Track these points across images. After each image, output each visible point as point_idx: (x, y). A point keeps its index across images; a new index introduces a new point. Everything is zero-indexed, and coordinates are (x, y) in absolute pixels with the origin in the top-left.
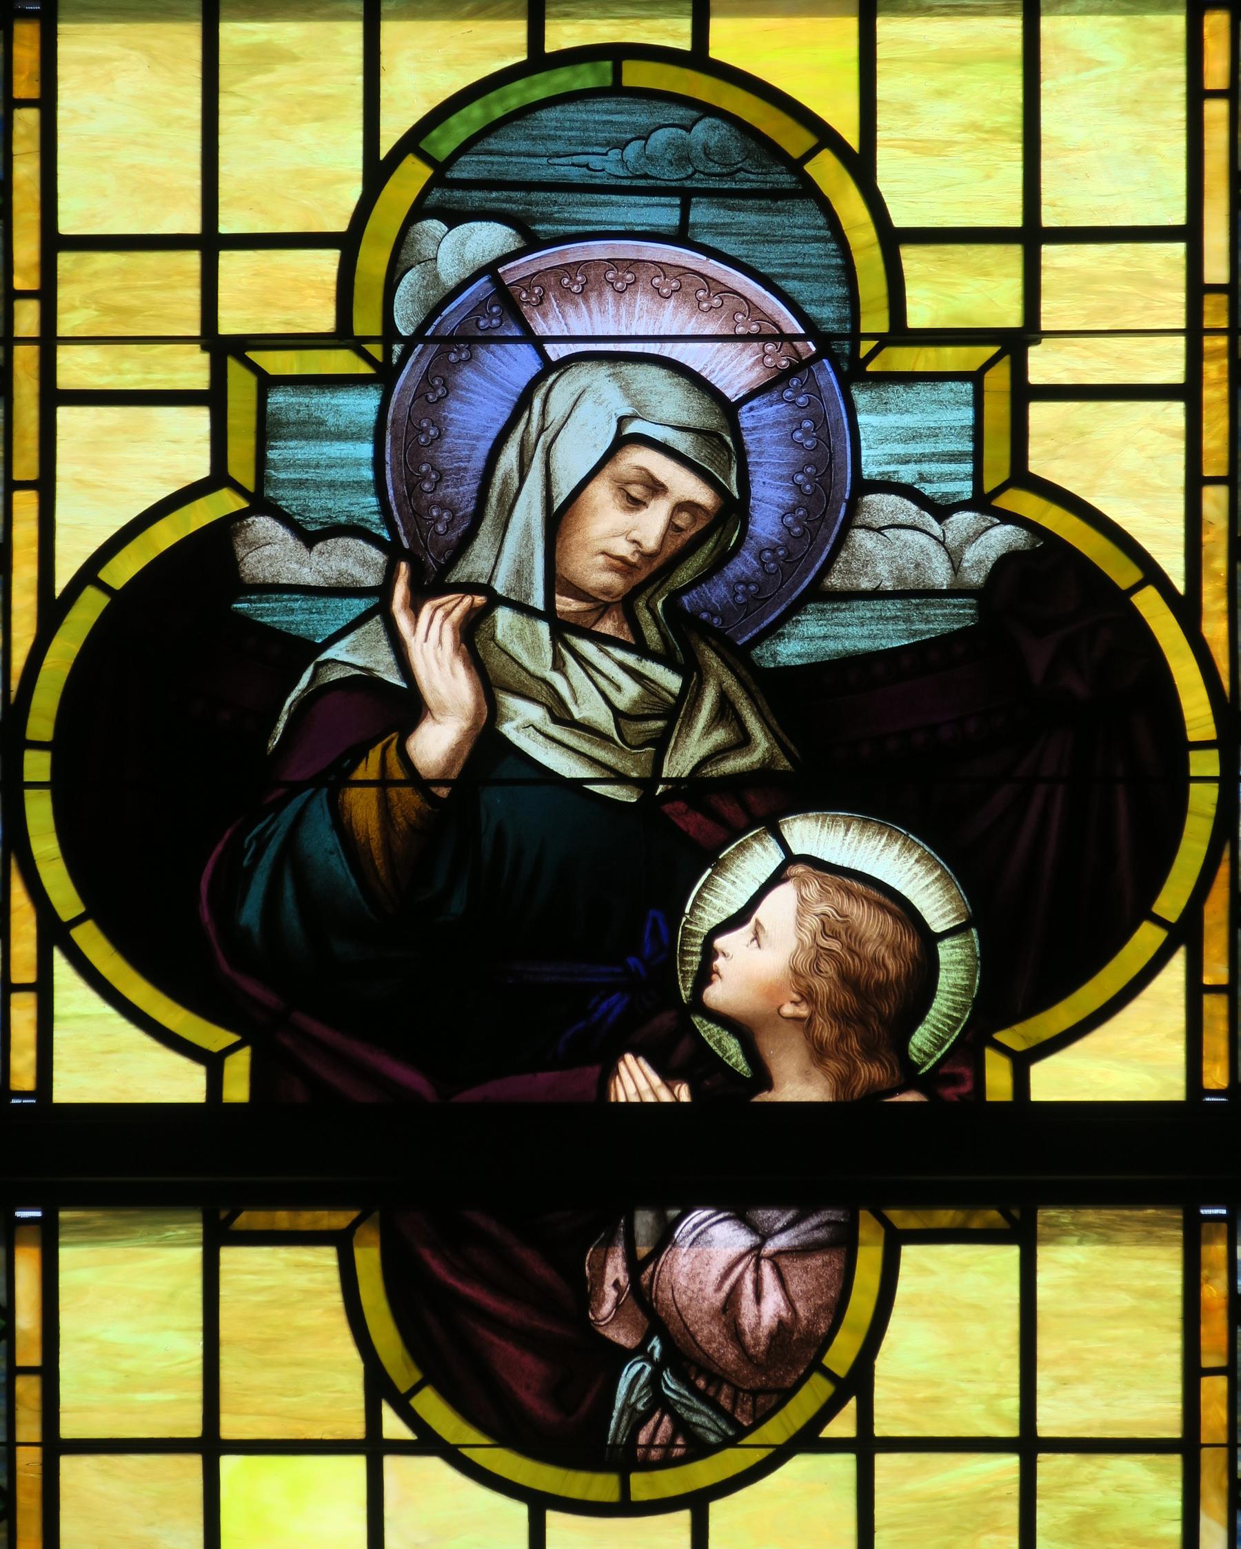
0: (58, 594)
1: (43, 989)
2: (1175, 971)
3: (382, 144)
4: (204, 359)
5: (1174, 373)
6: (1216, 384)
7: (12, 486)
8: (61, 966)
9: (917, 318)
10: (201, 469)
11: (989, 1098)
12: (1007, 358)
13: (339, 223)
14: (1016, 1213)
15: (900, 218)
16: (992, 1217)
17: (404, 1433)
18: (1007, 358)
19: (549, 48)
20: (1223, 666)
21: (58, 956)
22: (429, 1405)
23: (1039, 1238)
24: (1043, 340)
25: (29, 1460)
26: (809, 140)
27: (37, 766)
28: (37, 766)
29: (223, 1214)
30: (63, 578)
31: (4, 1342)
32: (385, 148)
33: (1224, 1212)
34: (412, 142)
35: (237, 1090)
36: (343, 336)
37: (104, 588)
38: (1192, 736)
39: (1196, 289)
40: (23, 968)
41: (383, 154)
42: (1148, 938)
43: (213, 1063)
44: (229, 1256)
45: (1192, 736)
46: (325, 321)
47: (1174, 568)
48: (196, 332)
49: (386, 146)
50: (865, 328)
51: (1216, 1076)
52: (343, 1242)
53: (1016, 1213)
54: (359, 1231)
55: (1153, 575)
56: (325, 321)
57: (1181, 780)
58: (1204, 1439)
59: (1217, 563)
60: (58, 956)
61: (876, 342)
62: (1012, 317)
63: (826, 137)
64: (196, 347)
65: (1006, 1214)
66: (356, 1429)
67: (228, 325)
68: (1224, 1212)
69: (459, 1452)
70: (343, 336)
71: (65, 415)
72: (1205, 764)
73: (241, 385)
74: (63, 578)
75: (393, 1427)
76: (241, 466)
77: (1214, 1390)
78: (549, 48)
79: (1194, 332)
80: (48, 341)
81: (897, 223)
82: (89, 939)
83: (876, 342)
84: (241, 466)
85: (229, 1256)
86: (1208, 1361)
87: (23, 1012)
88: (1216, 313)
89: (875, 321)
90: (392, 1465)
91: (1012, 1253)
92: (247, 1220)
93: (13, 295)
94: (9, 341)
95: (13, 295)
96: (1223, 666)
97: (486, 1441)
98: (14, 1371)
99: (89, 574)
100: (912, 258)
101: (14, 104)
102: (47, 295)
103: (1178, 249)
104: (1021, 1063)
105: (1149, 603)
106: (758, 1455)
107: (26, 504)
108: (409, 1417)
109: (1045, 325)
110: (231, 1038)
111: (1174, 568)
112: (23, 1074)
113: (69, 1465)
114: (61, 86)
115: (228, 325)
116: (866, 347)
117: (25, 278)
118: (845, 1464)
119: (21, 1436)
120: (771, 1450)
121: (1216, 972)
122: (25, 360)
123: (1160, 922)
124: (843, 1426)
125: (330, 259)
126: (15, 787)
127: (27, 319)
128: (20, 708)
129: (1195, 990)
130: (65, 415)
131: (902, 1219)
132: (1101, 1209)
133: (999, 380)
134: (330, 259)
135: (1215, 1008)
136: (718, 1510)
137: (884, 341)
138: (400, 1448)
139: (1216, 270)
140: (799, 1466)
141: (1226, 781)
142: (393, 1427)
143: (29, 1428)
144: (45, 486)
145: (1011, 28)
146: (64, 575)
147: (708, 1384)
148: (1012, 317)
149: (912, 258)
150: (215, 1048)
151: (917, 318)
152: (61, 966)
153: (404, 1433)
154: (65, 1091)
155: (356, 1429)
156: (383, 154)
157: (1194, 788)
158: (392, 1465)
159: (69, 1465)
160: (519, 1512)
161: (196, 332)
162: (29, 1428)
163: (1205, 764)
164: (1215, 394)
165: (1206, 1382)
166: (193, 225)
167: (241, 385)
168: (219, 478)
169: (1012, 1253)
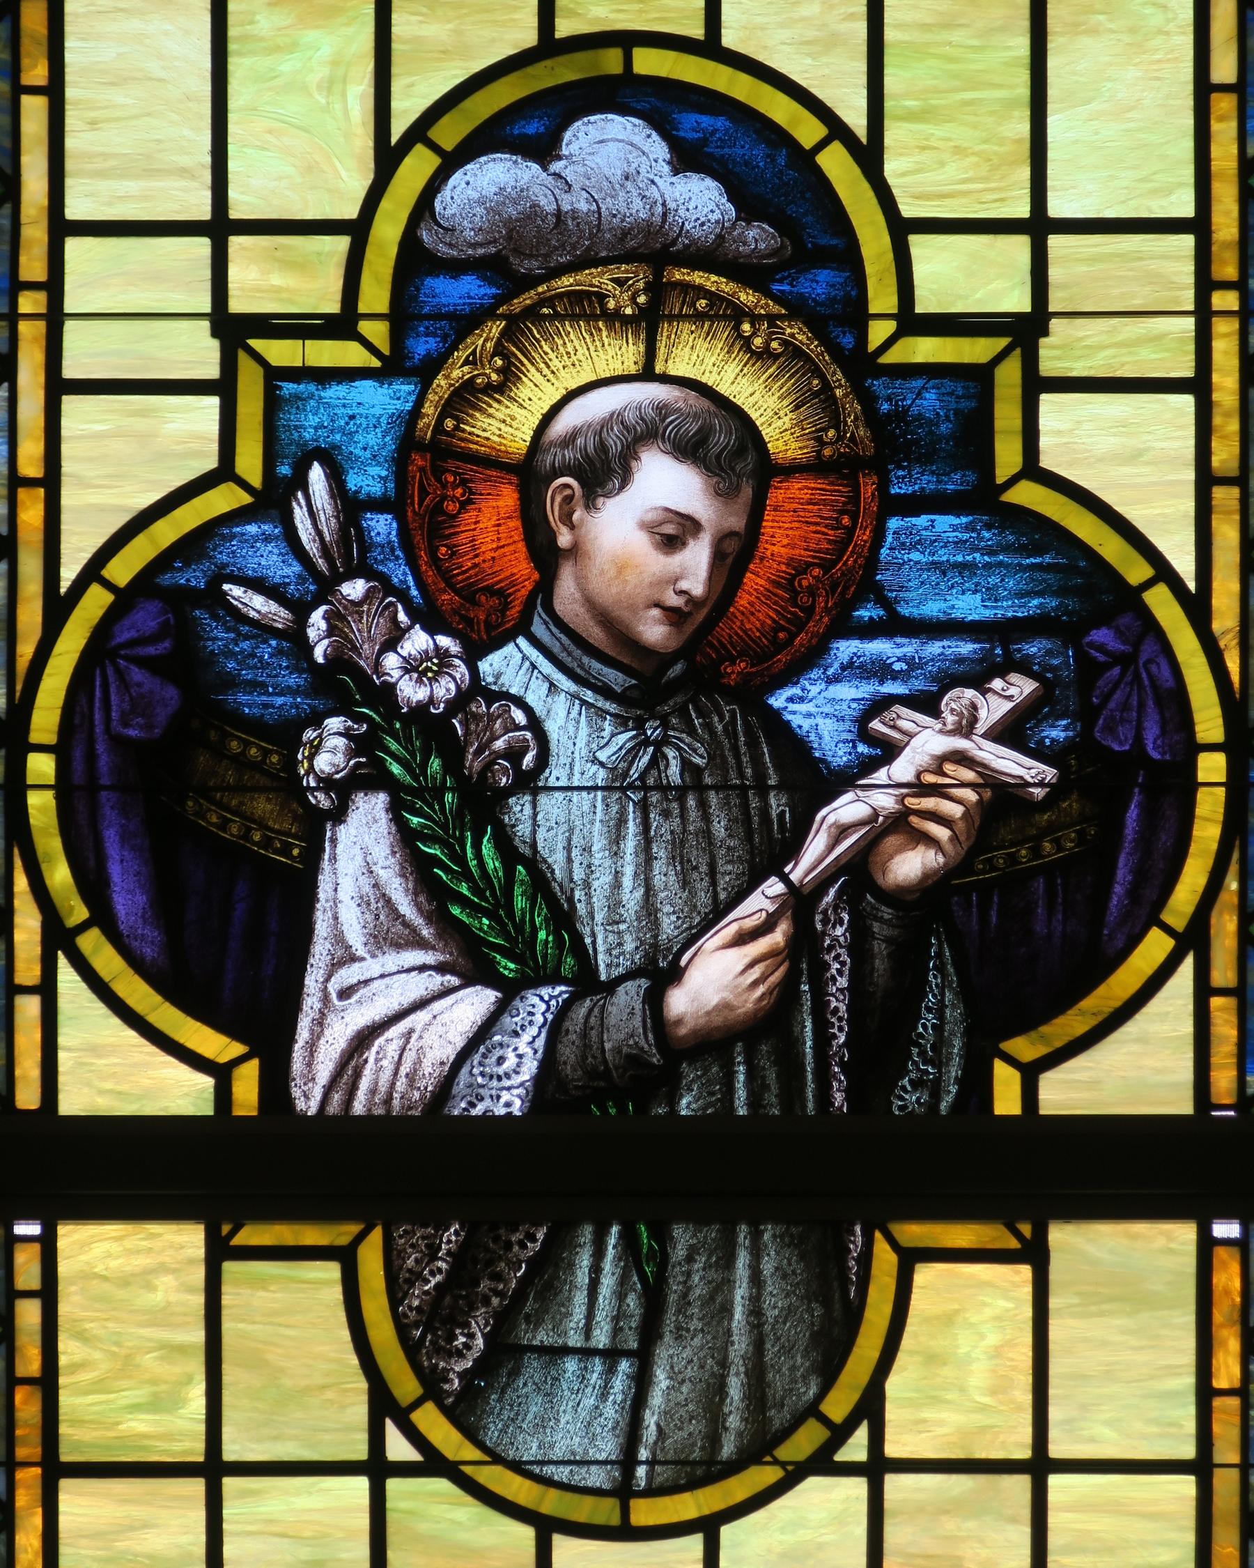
0: (63, 590)
1: (47, 990)
8: (67, 976)
11: (1042, 1112)
12: (1018, 352)
13: (351, 211)
14: (1026, 1229)
15: (908, 209)
18: (1018, 352)
21: (62, 961)
22: (430, 1420)
27: (41, 766)
28: (41, 766)
29: (226, 1229)
34: (419, 131)
36: (346, 1257)
37: (108, 585)
39: (1205, 284)
40: (28, 970)
42: (1155, 946)
43: (222, 1074)
44: (230, 1268)
47: (1184, 564)
51: (1224, 1081)
52: (346, 1257)
55: (1164, 572)
57: (1189, 786)
60: (62, 961)
62: (1018, 301)
63: (837, 129)
65: (1018, 1235)
67: (238, 304)
69: (460, 1470)
72: (1212, 767)
74: (68, 574)
75: (399, 1448)
79: (1204, 315)
80: (55, 318)
82: (93, 943)
85: (230, 1268)
86: (1220, 1382)
87: (29, 1008)
90: (394, 1486)
92: (250, 1235)
95: (15, 990)
98: (13, 1382)
99: (92, 572)
100: (920, 245)
101: (15, 990)
102: (54, 285)
103: (1187, 242)
104: (1030, 1074)
105: (1161, 603)
110: (238, 1049)
111: (1184, 564)
112: (28, 1097)
115: (238, 304)
117: (33, 266)
118: (858, 1487)
121: (1223, 972)
122: (31, 334)
124: (856, 1449)
125: (342, 243)
126: (17, 786)
128: (22, 707)
129: (1203, 990)
131: (914, 1233)
133: (1009, 376)
135: (1222, 1010)
138: (406, 1470)
141: (1235, 785)
142: (399, 1448)
143: (28, 1449)
149: (920, 245)
150: (223, 1059)
154: (71, 1103)
155: (359, 1450)
161: (206, 307)
162: (28, 1449)
163: (1212, 767)
165: (1217, 1402)
166: (203, 211)
168: (225, 472)
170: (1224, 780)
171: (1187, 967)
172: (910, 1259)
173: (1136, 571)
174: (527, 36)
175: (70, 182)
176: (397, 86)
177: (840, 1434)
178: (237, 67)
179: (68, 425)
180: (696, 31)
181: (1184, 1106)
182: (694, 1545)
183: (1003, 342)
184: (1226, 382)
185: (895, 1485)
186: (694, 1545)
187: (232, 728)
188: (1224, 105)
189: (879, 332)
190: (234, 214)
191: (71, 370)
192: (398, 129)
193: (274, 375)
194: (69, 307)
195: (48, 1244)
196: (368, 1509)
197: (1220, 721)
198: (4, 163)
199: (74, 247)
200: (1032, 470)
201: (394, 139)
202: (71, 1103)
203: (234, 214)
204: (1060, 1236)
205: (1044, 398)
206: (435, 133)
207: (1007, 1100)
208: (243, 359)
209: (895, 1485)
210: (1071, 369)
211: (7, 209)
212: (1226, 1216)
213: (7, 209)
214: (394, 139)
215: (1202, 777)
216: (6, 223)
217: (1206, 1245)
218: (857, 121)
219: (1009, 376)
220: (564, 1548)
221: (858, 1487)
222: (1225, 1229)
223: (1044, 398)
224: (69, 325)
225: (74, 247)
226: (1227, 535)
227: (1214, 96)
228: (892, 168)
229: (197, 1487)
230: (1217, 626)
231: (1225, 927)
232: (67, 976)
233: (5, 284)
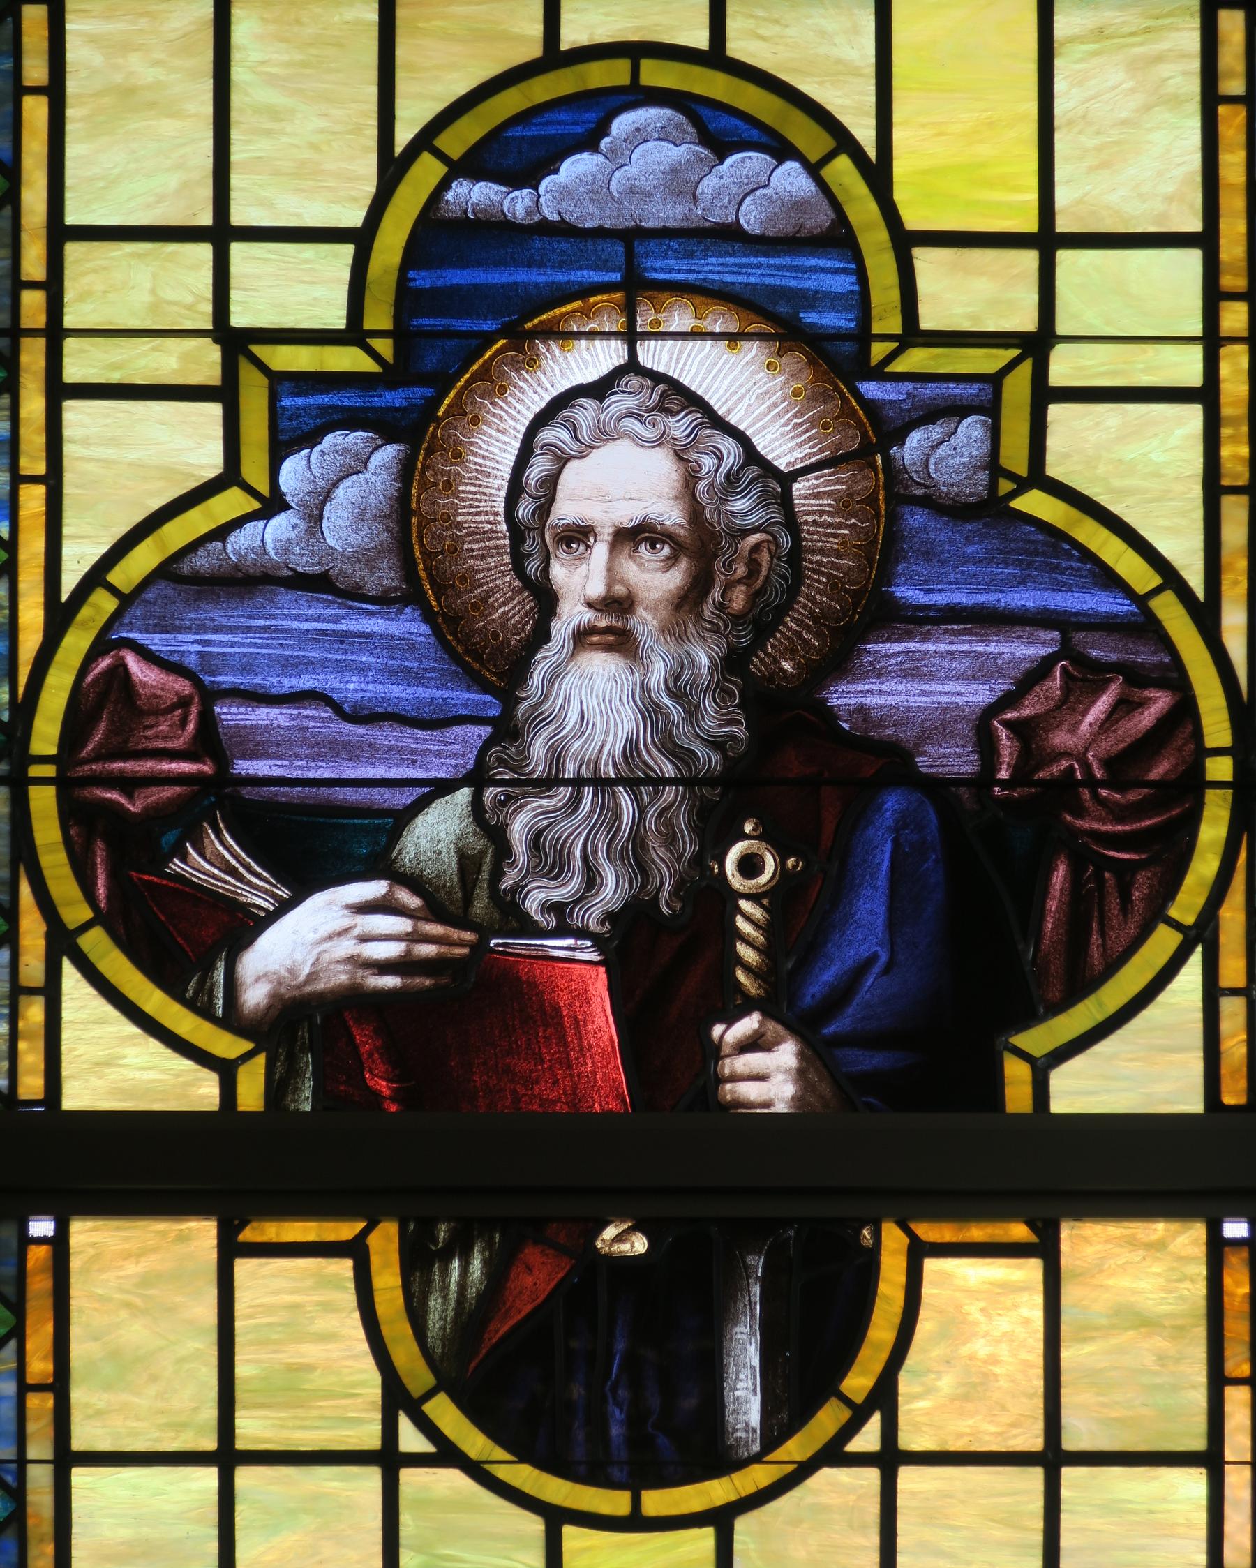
2: (1191, 976)
8: (71, 976)
9: (928, 321)
10: (210, 461)
13: (354, 217)
15: (913, 219)
16: (1019, 1232)
19: (564, 46)
22: (444, 1412)
30: (69, 582)
34: (425, 140)
35: (251, 1094)
36: (353, 334)
39: (1213, 296)
42: (1163, 941)
43: (226, 1071)
44: (244, 1268)
46: (337, 319)
48: (209, 325)
49: (399, 147)
52: (356, 1251)
56: (337, 319)
58: (1229, 1456)
62: (1025, 320)
67: (239, 318)
70: (353, 334)
75: (411, 1440)
78: (564, 46)
79: (1212, 341)
80: (55, 333)
82: (96, 943)
84: (254, 469)
85: (244, 1268)
88: (1234, 318)
89: (888, 321)
90: (409, 1477)
93: (20, 90)
94: (15, 332)
97: (508, 1457)
98: (19, 284)
99: (96, 577)
102: (54, 285)
104: (1041, 1070)
108: (427, 1427)
109: (1061, 328)
113: (80, 1477)
114: (1199, 1004)
115: (239, 318)
117: (34, 264)
118: (871, 1477)
119: (32, 1453)
120: (795, 1466)
121: (1233, 970)
122: (33, 355)
123: (1176, 925)
124: (868, 1439)
125: (346, 251)
127: (33, 304)
128: (25, 708)
132: (1121, 1221)
133: (1018, 387)
134: (346, 251)
135: (1233, 1012)
136: (743, 1526)
140: (826, 1475)
142: (411, 1440)
149: (926, 260)
152: (71, 976)
154: (74, 1098)
159: (80, 1477)
160: (534, 1526)
161: (209, 325)
168: (231, 476)
170: (1226, 1466)
171: (1195, 960)
172: (918, 1252)
174: (534, 50)
177: (851, 1428)
180: (571, 1534)
181: (1194, 1105)
182: (703, 1540)
183: (1015, 353)
184: (1233, 230)
185: (908, 1478)
186: (703, 1540)
187: (225, 827)
189: (879, 350)
192: (403, 136)
193: (279, 381)
194: (69, 321)
195: (60, 1244)
197: (1227, 725)
199: (73, 250)
201: (398, 149)
202: (74, 1098)
204: (1068, 1232)
207: (1018, 1097)
209: (908, 1478)
211: (7, 211)
212: (1236, 1214)
213: (7, 211)
214: (398, 149)
216: (6, 224)
217: (1217, 1247)
219: (1018, 387)
221: (871, 1477)
222: (1235, 1229)
224: (70, 344)
226: (1234, 533)
231: (1233, 917)
233: (7, 283)
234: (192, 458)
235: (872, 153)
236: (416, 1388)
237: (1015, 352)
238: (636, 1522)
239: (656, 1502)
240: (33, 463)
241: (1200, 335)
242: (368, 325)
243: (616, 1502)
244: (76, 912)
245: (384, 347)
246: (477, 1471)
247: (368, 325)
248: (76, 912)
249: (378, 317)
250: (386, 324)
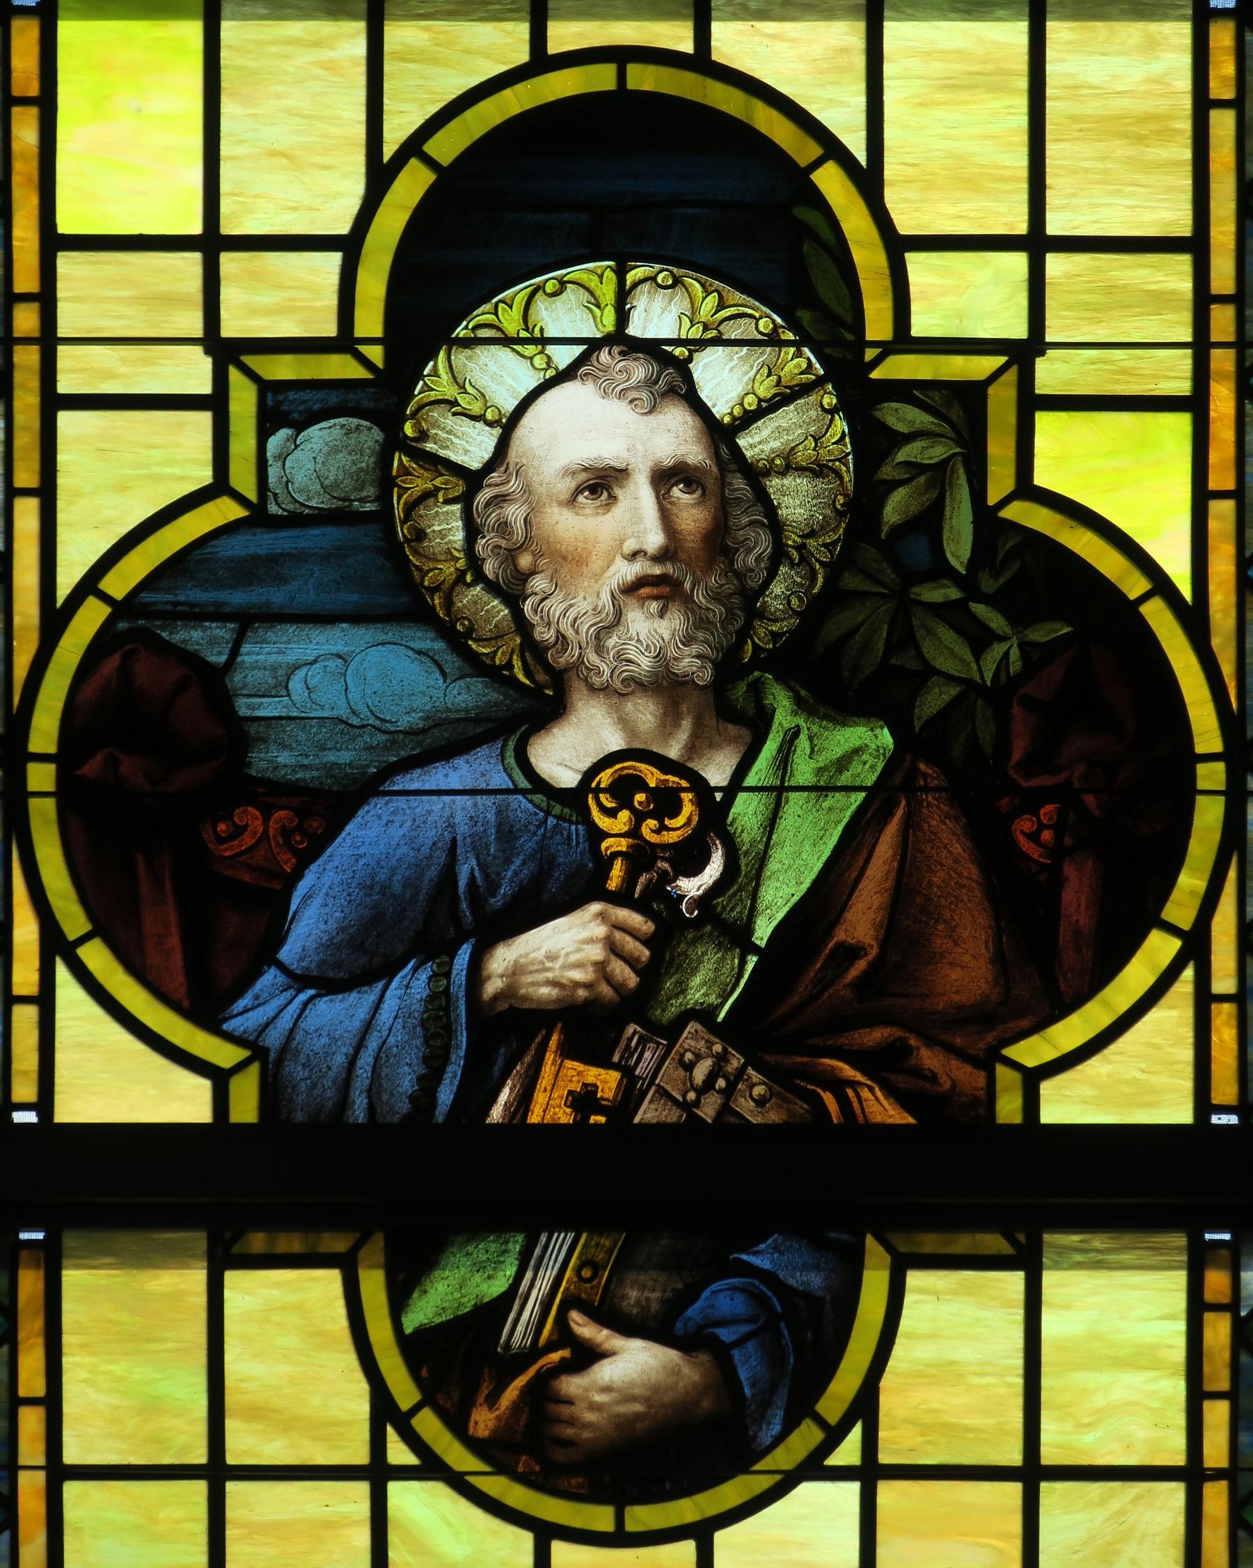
1: (45, 1000)
3: (385, 149)
4: (206, 363)
5: (1183, 387)
6: (1195, 871)
7: (12, 492)
8: (67, 988)
9: (921, 326)
10: (204, 475)
13: (344, 228)
14: (1021, 1238)
15: (906, 225)
16: (995, 1243)
17: (409, 1458)
20: (1228, 669)
22: (428, 1424)
23: (1044, 1267)
24: (1048, 351)
25: (31, 1486)
26: (815, 151)
27: (41, 777)
28: (41, 777)
30: (66, 584)
31: (5, 1349)
32: (389, 151)
33: (1227, 1237)
34: (414, 146)
36: (345, 342)
37: (105, 598)
38: (1200, 749)
39: (1203, 299)
40: (25, 977)
41: (386, 158)
43: (220, 1079)
45: (1200, 749)
47: (1180, 575)
49: (389, 151)
50: (870, 336)
51: (1225, 1089)
53: (1021, 1238)
54: (362, 1254)
55: (1161, 584)
57: (1187, 794)
59: (1222, 566)
61: (880, 350)
62: (1019, 331)
64: (198, 350)
66: (359, 1455)
67: (230, 328)
68: (1227, 1237)
71: (65, 419)
72: (1211, 775)
73: (243, 399)
74: (66, 584)
75: (399, 1453)
76: (243, 478)
77: (1217, 1414)
79: (1201, 346)
80: (48, 340)
81: (903, 231)
82: (96, 956)
83: (880, 350)
84: (243, 478)
87: (25, 1019)
88: (1223, 321)
90: (397, 1491)
91: (1015, 1281)
94: (9, 341)
96: (1228, 669)
99: (89, 585)
100: (918, 265)
102: (47, 299)
104: (1033, 1078)
105: (1157, 615)
106: (764, 1483)
107: (27, 514)
108: (413, 1440)
111: (1180, 575)
113: (71, 1489)
115: (230, 328)
116: (870, 354)
117: (26, 279)
120: (778, 1477)
121: (1224, 982)
122: (27, 359)
124: (848, 1452)
125: (334, 260)
126: (18, 795)
127: (26, 320)
130: (65, 419)
134: (334, 260)
135: (1224, 1022)
136: (722, 1538)
137: (887, 349)
138: (404, 1473)
139: (1223, 276)
140: (807, 1491)
142: (399, 1453)
143: (31, 1449)
144: (47, 493)
145: (1016, 33)
146: (67, 580)
147: (720, 1091)
148: (1019, 331)
149: (918, 265)
151: (921, 326)
153: (409, 1458)
154: (68, 1111)
155: (359, 1455)
156: (386, 158)
157: (1201, 801)
158: (397, 1491)
160: (526, 1539)
161: (199, 333)
163: (1211, 775)
164: (1223, 399)
167: (243, 399)
168: (220, 486)
169: (1015, 1281)
170: (1223, 788)
173: (1135, 585)
175: (67, 1361)
176: (389, 104)
177: (835, 1436)
178: (229, 108)
179: (71, 1513)
182: (687, 1550)
183: (1002, 360)
186: (687, 1550)
188: (1224, 1016)
190: (231, 1459)
191: (65, 385)
193: (266, 388)
194: (64, 329)
196: (364, 62)
198: (5, 1489)
199: (66, 263)
200: (1026, 489)
203: (231, 1459)
205: (1044, 1486)
206: (432, 147)
207: (1009, 1109)
208: (234, 374)
209: (887, 1492)
210: (1071, 29)
213: (6, 1535)
215: (1201, 784)
218: (858, 147)
220: (560, 1550)
223: (1044, 1486)
224: (62, 350)
225: (66, 263)
227: (1215, 1007)
228: (892, 198)
229: (199, 1488)
230: (1216, 642)
232: (67, 988)
234: (523, 58)
235: (862, 157)
236: (405, 1404)
237: (1002, 360)
238: (620, 1538)
239: (642, 1517)
240: (26, 476)
241: (1189, 339)
242: (359, 333)
243: (601, 1518)
244: (74, 921)
245: (375, 354)
246: (460, 1484)
247: (359, 333)
248: (74, 921)
249: (369, 322)
250: (377, 331)
